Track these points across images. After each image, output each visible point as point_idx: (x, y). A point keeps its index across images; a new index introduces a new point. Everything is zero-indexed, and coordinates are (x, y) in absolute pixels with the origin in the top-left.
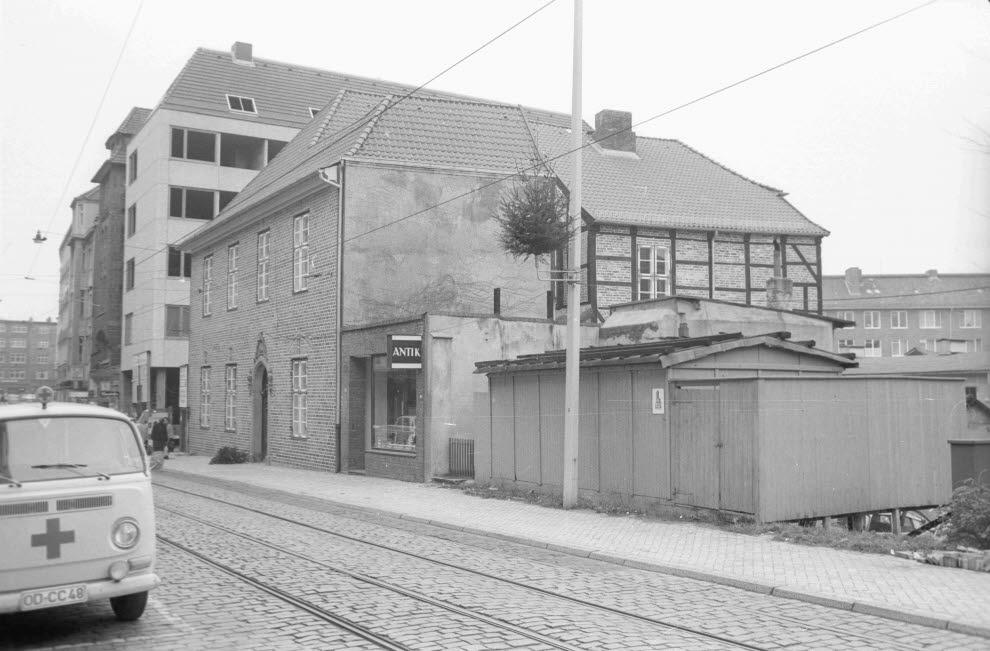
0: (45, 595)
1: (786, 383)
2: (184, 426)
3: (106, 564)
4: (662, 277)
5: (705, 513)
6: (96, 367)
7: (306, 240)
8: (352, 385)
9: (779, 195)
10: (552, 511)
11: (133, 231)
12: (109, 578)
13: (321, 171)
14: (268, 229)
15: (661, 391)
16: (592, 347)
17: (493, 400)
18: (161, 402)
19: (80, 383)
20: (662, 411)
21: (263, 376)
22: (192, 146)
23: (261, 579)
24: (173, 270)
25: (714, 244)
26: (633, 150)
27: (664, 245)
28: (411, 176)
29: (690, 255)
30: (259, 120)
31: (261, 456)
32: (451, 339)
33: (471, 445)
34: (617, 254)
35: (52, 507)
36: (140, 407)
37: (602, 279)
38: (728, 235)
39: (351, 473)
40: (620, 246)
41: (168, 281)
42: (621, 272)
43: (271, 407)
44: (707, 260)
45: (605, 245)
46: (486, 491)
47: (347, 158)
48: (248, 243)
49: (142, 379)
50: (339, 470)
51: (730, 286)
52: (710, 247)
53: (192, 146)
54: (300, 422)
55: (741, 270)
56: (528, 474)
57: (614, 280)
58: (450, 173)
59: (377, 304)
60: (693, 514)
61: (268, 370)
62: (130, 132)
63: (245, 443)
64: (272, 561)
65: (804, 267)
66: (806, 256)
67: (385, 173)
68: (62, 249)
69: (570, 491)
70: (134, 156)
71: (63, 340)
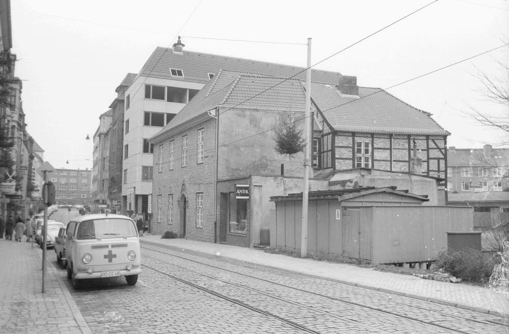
0: (108, 273)
1: (394, 209)
2: (150, 221)
3: (125, 266)
4: (367, 155)
5: (354, 260)
6: (110, 193)
7: (203, 141)
9: (428, 115)
10: (297, 259)
11: (127, 131)
12: (127, 269)
13: (209, 112)
14: (187, 135)
15: (339, 210)
16: (319, 191)
17: (277, 213)
18: (140, 211)
19: (103, 201)
20: (339, 219)
21: (184, 201)
22: (155, 93)
23: (176, 277)
24: (146, 150)
25: (392, 140)
26: (358, 94)
27: (368, 140)
28: (248, 113)
30: (185, 80)
31: (183, 235)
32: (261, 186)
33: (268, 232)
35: (110, 246)
36: (130, 213)
37: (338, 157)
38: (400, 135)
39: (220, 243)
40: (348, 141)
41: (146, 101)
42: (348, 153)
43: (187, 214)
44: (389, 147)
45: (339, 141)
46: (273, 251)
47: (220, 106)
48: (178, 139)
49: (131, 200)
50: (215, 242)
51: (401, 160)
52: (391, 142)
53: (155, 93)
54: (199, 221)
55: (406, 152)
56: (290, 245)
57: (343, 157)
58: (266, 111)
59: (233, 169)
60: (350, 261)
61: (186, 197)
62: (127, 85)
63: (176, 230)
64: (181, 272)
65: (438, 150)
66: (439, 145)
67: (236, 112)
69: (304, 251)
70: (128, 97)
71: (95, 180)
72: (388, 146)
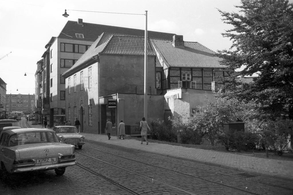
8: (102, 112)
29: (197, 75)
34: (176, 75)
37: (172, 82)
44: (202, 76)
50: (99, 134)
51: (208, 83)
68: (37, 64)
72: (201, 75)
